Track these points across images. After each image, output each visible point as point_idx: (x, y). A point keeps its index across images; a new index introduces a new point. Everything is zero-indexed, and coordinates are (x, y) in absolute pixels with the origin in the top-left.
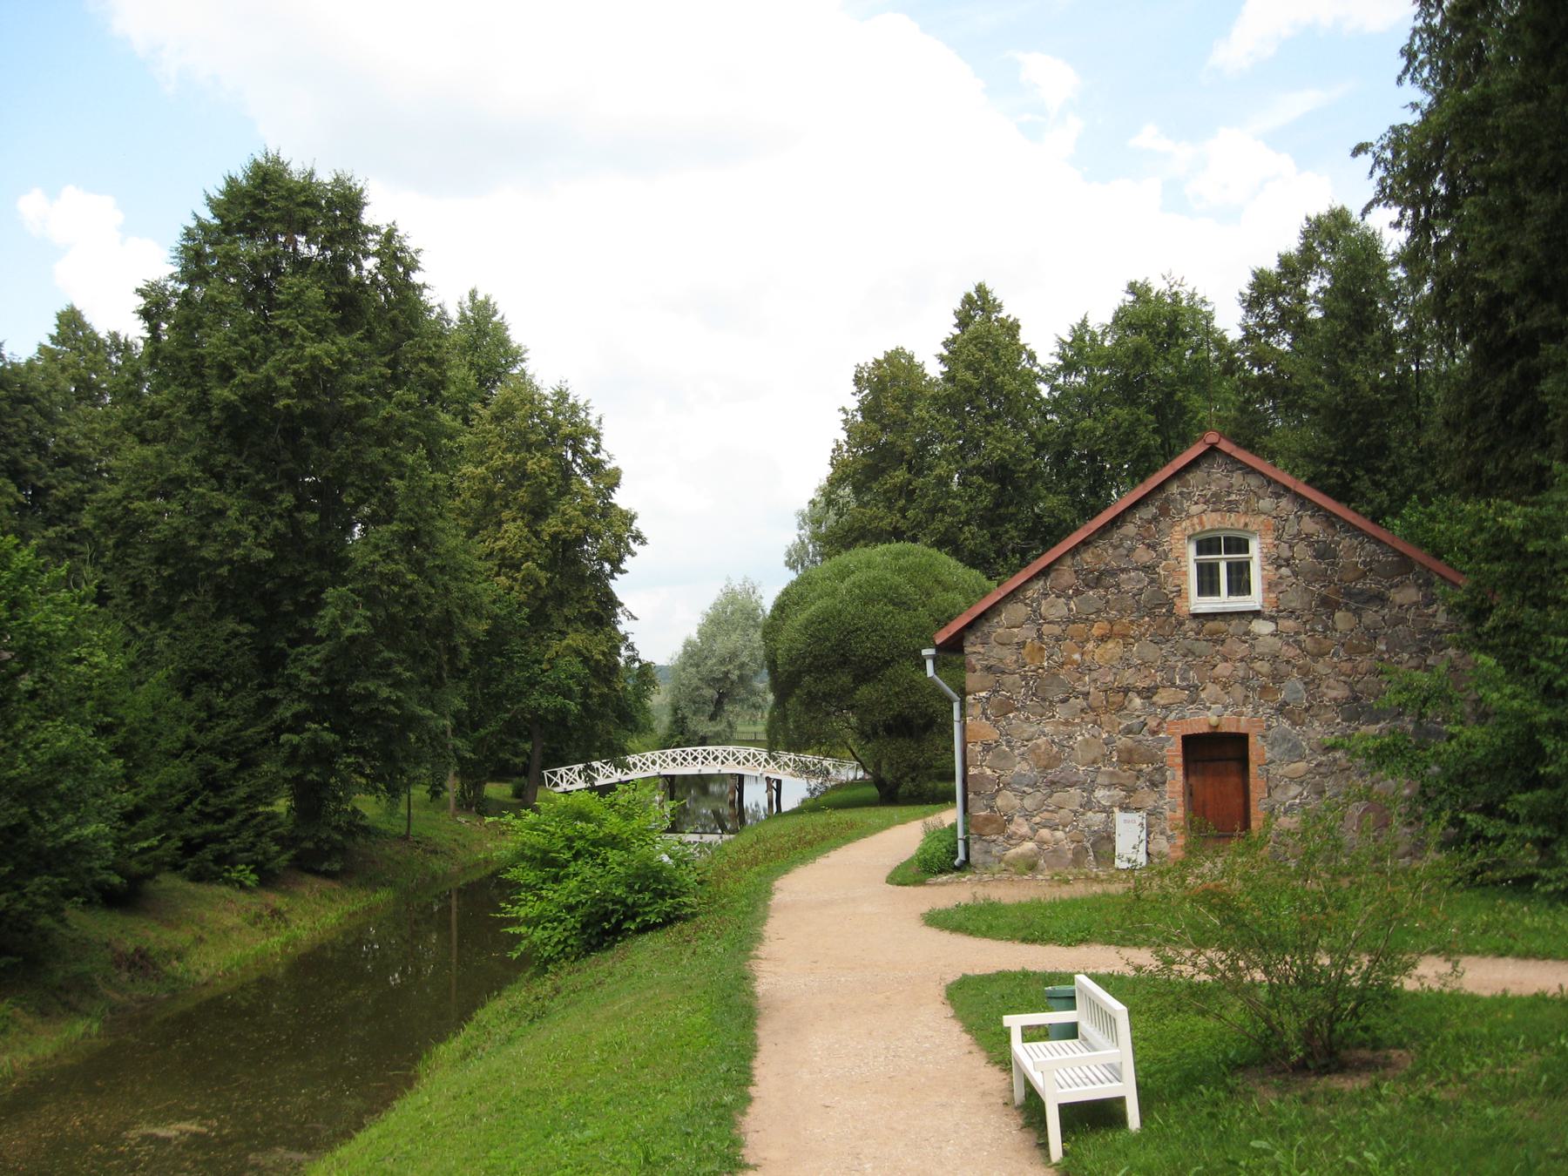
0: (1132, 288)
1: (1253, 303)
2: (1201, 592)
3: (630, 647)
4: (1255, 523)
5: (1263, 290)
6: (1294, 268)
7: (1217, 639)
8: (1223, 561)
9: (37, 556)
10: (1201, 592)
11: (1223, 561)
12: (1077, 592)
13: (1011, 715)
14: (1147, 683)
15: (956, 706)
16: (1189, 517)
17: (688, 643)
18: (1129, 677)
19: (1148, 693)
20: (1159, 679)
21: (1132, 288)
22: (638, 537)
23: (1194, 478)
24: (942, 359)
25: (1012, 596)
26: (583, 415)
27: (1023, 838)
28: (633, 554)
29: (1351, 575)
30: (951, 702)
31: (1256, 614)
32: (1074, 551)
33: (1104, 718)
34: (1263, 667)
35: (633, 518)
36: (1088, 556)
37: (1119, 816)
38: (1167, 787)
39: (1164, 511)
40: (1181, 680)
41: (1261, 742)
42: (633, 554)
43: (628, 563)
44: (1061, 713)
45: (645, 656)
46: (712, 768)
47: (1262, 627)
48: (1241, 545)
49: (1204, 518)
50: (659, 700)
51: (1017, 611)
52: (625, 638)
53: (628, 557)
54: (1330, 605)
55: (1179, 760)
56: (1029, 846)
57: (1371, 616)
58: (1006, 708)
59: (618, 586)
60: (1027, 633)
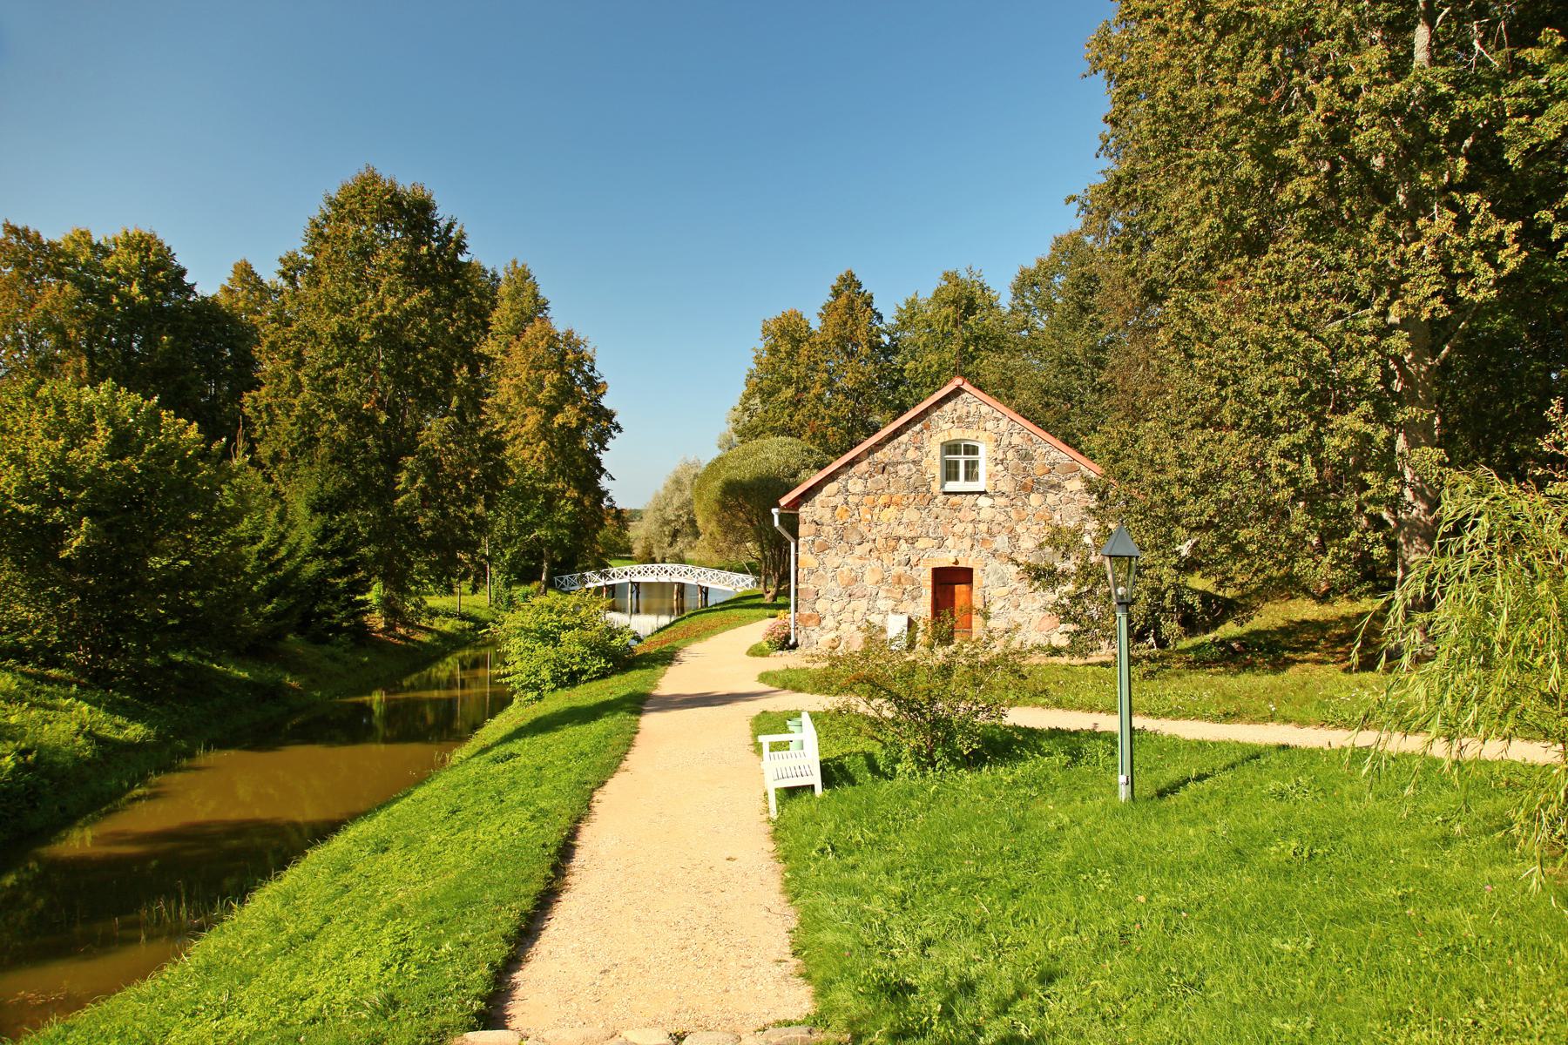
0: (947, 276)
1: (1018, 291)
3: (610, 499)
4: (983, 436)
5: (1026, 283)
6: (1047, 270)
7: (956, 508)
8: (962, 459)
9: (1295, 124)
12: (871, 476)
14: (913, 534)
15: (793, 545)
17: (657, 496)
18: (901, 531)
19: (912, 541)
21: (947, 276)
22: (618, 427)
23: (948, 407)
24: (821, 315)
25: (832, 477)
26: (582, 347)
28: (614, 438)
29: (1041, 472)
30: (789, 544)
32: (871, 451)
33: (884, 555)
34: (983, 527)
35: (613, 416)
36: (879, 456)
37: (891, 617)
41: (981, 574)
42: (614, 438)
43: (610, 444)
44: (859, 550)
45: (619, 506)
46: (664, 579)
47: (983, 501)
50: (637, 533)
51: (831, 488)
52: (606, 493)
53: (610, 440)
54: (1027, 489)
55: (930, 583)
57: (1051, 498)
58: (825, 548)
59: (605, 458)
60: (839, 500)
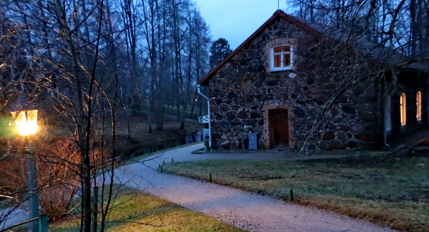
2: (275, 66)
10: (275, 66)
11: (282, 55)
13: (221, 104)
16: (271, 40)
20: (261, 93)
27: (225, 140)
31: (291, 71)
38: (264, 125)
39: (264, 39)
40: (268, 93)
48: (287, 49)
49: (276, 40)
56: (227, 142)
